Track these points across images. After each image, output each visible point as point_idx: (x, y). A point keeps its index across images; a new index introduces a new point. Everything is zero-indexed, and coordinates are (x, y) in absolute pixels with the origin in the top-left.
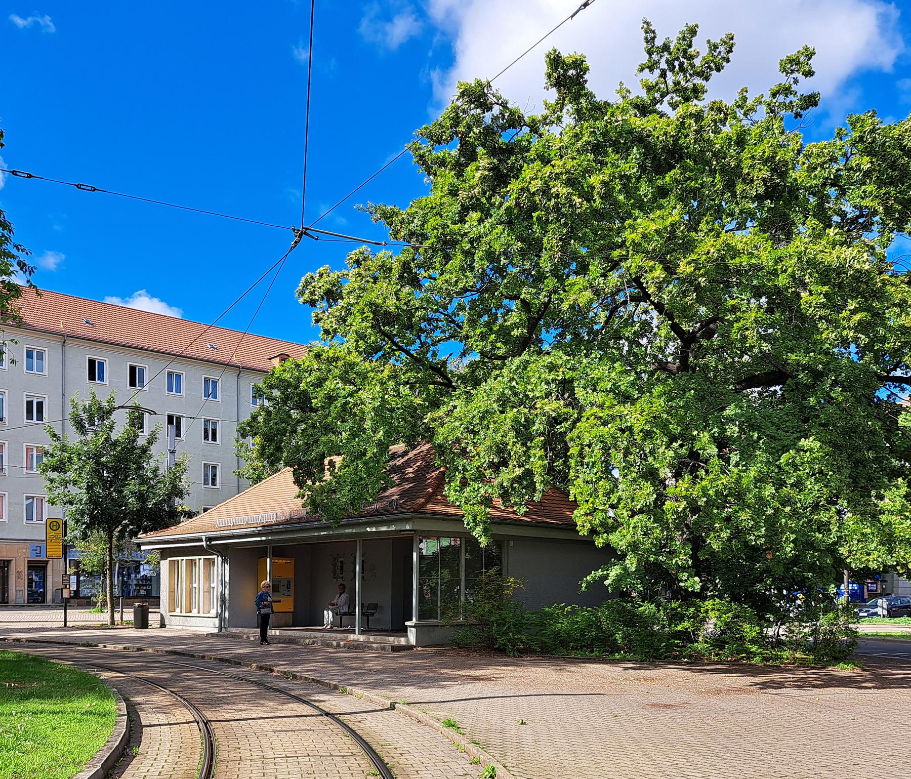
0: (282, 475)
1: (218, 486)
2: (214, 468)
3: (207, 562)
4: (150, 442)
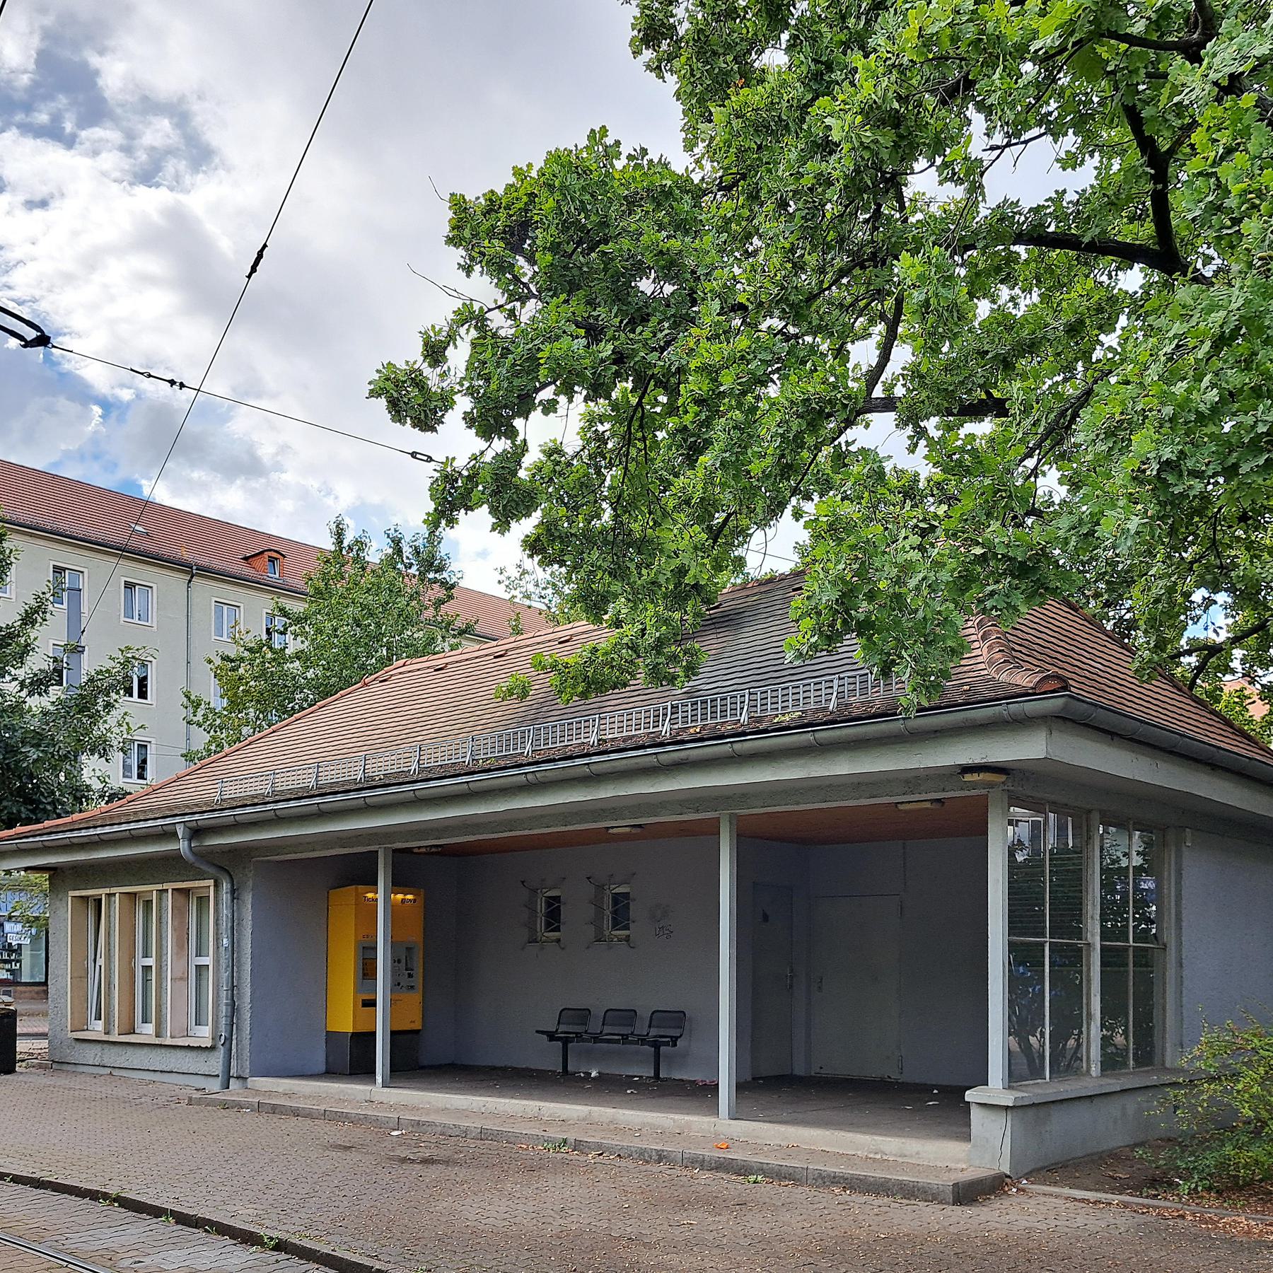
0: (364, 691)
2: (142, 747)
3: (181, 899)
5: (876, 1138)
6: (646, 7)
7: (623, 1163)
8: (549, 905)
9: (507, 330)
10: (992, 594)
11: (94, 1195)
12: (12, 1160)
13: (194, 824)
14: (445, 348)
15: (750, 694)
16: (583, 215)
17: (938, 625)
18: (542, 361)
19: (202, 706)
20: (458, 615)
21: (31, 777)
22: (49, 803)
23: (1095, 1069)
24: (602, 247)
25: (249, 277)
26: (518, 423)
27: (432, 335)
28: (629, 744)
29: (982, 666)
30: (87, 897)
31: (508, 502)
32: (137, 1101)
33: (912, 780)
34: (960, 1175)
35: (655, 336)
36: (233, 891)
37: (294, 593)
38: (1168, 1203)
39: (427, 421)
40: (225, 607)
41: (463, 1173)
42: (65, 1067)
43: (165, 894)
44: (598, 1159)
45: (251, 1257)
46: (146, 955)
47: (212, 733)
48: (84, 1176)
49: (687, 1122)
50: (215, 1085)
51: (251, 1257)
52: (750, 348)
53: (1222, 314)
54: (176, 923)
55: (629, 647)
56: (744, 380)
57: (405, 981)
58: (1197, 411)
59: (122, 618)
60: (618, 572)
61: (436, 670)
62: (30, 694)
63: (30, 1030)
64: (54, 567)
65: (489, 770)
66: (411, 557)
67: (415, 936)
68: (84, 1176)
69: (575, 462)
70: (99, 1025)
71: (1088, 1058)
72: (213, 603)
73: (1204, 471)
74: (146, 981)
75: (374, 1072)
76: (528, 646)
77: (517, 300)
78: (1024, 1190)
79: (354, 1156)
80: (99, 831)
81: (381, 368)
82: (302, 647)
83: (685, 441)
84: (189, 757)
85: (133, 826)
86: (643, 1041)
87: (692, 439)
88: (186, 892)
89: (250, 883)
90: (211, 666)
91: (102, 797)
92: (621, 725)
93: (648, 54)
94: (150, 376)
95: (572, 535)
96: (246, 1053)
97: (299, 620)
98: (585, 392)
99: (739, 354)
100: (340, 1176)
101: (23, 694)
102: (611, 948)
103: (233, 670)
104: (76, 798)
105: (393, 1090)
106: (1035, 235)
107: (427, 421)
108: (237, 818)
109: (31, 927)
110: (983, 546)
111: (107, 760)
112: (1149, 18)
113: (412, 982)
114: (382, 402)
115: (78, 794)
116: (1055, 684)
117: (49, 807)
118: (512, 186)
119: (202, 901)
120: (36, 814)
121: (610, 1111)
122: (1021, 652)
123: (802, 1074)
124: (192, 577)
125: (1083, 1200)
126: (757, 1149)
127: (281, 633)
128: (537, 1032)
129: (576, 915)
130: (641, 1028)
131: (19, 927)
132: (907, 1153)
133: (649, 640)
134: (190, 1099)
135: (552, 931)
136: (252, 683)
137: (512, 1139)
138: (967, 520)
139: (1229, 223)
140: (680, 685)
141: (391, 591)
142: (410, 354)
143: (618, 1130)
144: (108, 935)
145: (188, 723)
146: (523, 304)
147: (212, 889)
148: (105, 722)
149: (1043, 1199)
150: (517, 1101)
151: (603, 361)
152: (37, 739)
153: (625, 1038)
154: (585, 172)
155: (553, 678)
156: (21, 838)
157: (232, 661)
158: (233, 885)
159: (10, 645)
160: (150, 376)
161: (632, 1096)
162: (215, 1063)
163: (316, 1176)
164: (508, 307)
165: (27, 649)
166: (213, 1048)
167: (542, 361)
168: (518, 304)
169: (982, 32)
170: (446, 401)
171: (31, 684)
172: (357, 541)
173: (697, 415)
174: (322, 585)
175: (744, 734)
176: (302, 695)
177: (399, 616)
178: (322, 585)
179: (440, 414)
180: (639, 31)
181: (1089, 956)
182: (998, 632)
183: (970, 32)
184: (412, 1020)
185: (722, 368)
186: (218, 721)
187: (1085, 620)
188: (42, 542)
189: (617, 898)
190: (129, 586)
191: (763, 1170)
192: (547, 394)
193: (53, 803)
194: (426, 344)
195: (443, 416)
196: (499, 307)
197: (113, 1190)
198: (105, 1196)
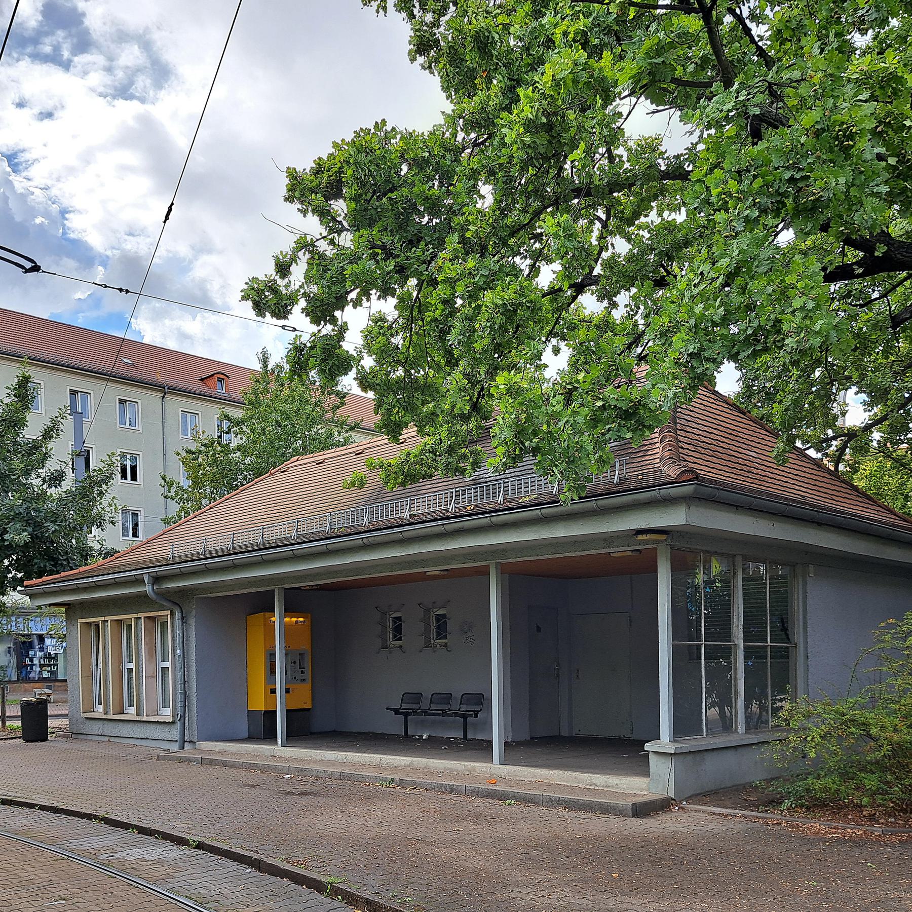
0: (271, 479)
1: (140, 538)
2: (135, 515)
3: (150, 624)
4: (47, 435)
5: (590, 775)
6: (417, 30)
7: (428, 794)
8: (395, 623)
9: (330, 252)
10: (609, 430)
11: (89, 817)
12: (39, 796)
13: (155, 574)
14: (290, 266)
15: (504, 483)
16: (371, 179)
17: (577, 451)
18: (347, 276)
19: (174, 486)
20: (349, 416)
21: (52, 542)
22: (64, 560)
23: (741, 729)
24: (390, 195)
25: (165, 222)
26: (337, 314)
27: (281, 257)
28: (428, 518)
29: (658, 461)
30: (90, 623)
31: (332, 366)
32: (124, 758)
33: (609, 539)
34: (640, 798)
35: (423, 254)
36: (183, 618)
37: (235, 403)
38: (772, 816)
39: (281, 312)
40: (189, 415)
41: (322, 800)
42: (80, 737)
43: (139, 621)
44: (413, 791)
45: (181, 853)
46: (130, 661)
47: (182, 504)
48: (84, 805)
49: (473, 767)
50: (175, 747)
51: (181, 853)
52: (475, 266)
53: (727, 260)
54: (147, 640)
55: (430, 452)
56: (470, 288)
57: (299, 676)
58: (712, 320)
59: (118, 425)
60: (409, 407)
61: (317, 464)
62: (50, 486)
63: (56, 713)
64: (71, 390)
65: (340, 536)
66: (315, 376)
67: (305, 645)
68: (84, 805)
69: (394, 326)
70: (101, 708)
71: (736, 721)
72: (180, 412)
73: (716, 358)
74: (130, 678)
75: (276, 737)
76: (377, 446)
77: (335, 232)
78: (683, 808)
79: (256, 791)
80: (95, 579)
81: (248, 281)
82: (241, 442)
83: (437, 327)
84: (166, 521)
85: (116, 576)
86: (456, 715)
87: (441, 326)
88: (153, 619)
89: (194, 613)
90: (179, 457)
91: (100, 554)
92: (429, 503)
93: (421, 59)
94: (106, 286)
95: (377, 385)
96: (195, 726)
97: (239, 423)
98: (378, 294)
99: (468, 271)
100: (245, 803)
101: (45, 487)
102: (435, 651)
103: (194, 459)
104: (82, 556)
105: (288, 749)
106: (677, 174)
107: (281, 312)
108: (182, 569)
109: (62, 641)
110: (603, 400)
111: (102, 530)
112: (696, 63)
113: (304, 676)
114: (249, 303)
115: (84, 553)
116: (690, 476)
117: (64, 563)
118: (332, 155)
119: (164, 625)
120: (56, 568)
121: (424, 760)
122: (688, 449)
123: (567, 735)
124: (165, 394)
125: (719, 814)
126: (517, 783)
127: (227, 433)
128: (387, 709)
129: (413, 629)
130: (455, 706)
131: (54, 642)
132: (610, 785)
133: (444, 446)
134: (158, 756)
135: (396, 640)
136: (208, 468)
137: (360, 779)
138: (594, 383)
139: (713, 212)
140: (469, 475)
141: (301, 401)
142: (266, 270)
143: (428, 772)
144: (104, 647)
145: (165, 497)
146: (339, 235)
147: (169, 616)
148: (101, 503)
149: (693, 813)
150: (366, 755)
151: (388, 273)
152: (55, 517)
153: (444, 713)
154: (371, 151)
155: (381, 474)
156: (46, 585)
157: (193, 453)
158: (182, 612)
159: (35, 454)
160: (106, 286)
161: (446, 751)
162: (174, 733)
163: (230, 804)
164: (330, 237)
165: (46, 456)
166: (173, 723)
167: (347, 276)
168: (336, 235)
169: (591, 76)
170: (293, 299)
171: (50, 480)
172: (277, 366)
173: (443, 310)
174: (254, 398)
175: (499, 511)
176: (243, 476)
177: (307, 418)
178: (254, 398)
179: (289, 308)
180: (414, 45)
181: (735, 653)
182: (671, 436)
183: (584, 77)
184: (304, 700)
185: (458, 280)
186: (185, 496)
187: (751, 420)
188: (61, 374)
189: (439, 618)
190: (122, 402)
191: (515, 797)
192: (353, 295)
193: (67, 560)
194: (277, 264)
195: (291, 309)
196: (324, 237)
197: (100, 814)
198: (96, 817)
